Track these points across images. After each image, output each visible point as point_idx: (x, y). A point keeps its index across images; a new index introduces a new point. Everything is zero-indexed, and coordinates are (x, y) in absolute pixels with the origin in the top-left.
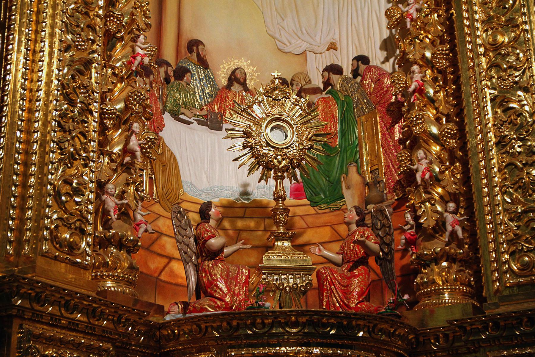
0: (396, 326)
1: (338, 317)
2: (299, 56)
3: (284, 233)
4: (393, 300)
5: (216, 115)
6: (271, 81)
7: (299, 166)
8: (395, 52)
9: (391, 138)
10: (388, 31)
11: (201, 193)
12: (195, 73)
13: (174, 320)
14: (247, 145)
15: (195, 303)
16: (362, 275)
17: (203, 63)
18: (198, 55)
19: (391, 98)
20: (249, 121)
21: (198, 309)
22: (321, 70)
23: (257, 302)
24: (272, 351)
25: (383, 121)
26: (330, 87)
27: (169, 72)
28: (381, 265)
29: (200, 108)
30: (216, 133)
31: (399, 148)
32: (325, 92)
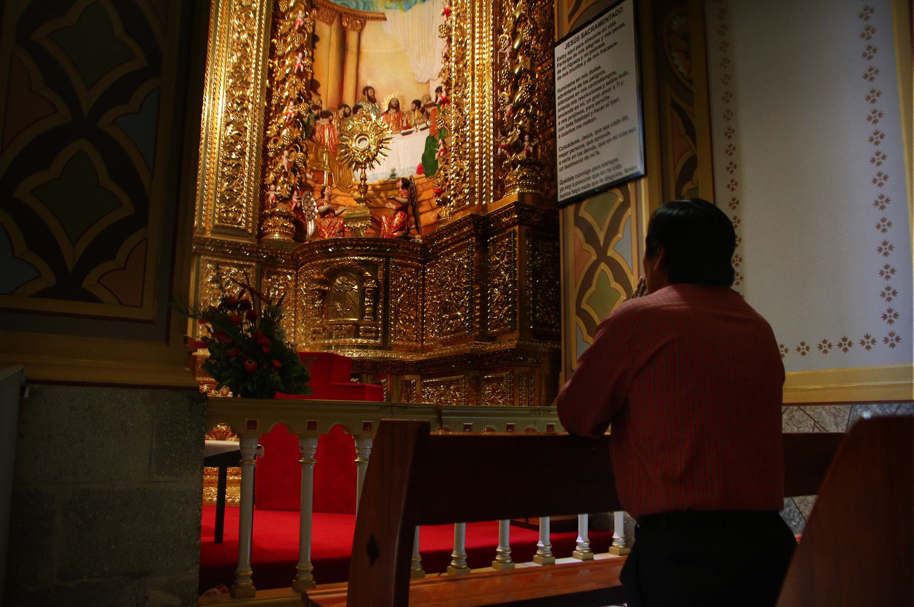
17: (372, 100)
27: (346, 111)
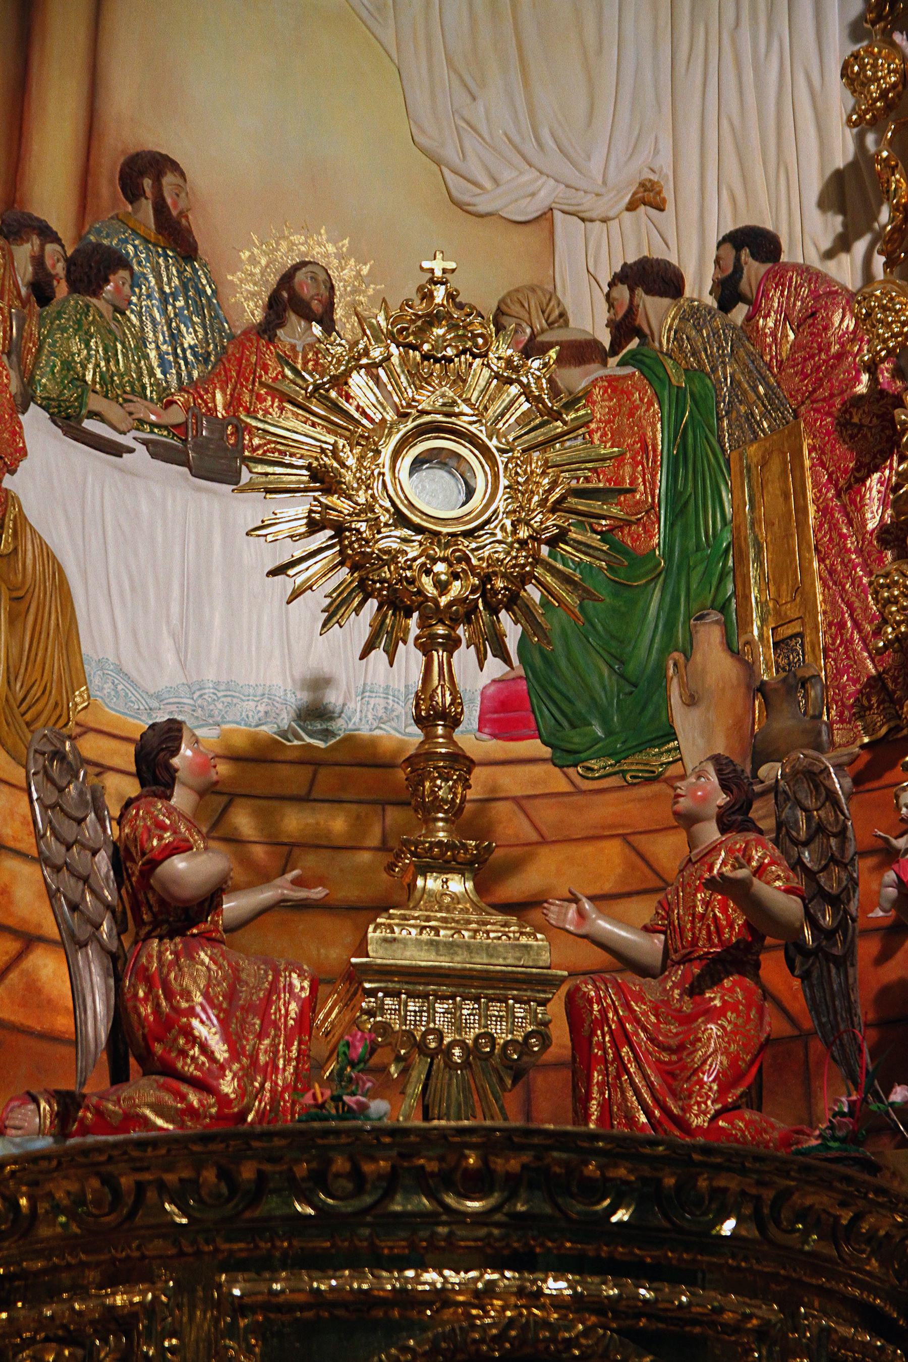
0: (861, 1203)
1: (644, 1158)
2: (527, 229)
3: (449, 846)
4: (852, 1104)
5: (219, 425)
6: (420, 289)
7: (513, 602)
8: (875, 218)
9: (850, 523)
10: (849, 134)
11: (154, 704)
12: (147, 271)
13: (15, 1160)
14: (323, 519)
15: (103, 1097)
16: (735, 1010)
18: (160, 208)
19: (857, 379)
20: (336, 434)
21: (115, 1122)
22: (605, 278)
23: (337, 1099)
24: (389, 1283)
25: (823, 465)
26: (636, 341)
27: (48, 262)
28: (805, 977)
29: (160, 400)
30: (215, 493)
31: (881, 560)
32: (617, 359)
